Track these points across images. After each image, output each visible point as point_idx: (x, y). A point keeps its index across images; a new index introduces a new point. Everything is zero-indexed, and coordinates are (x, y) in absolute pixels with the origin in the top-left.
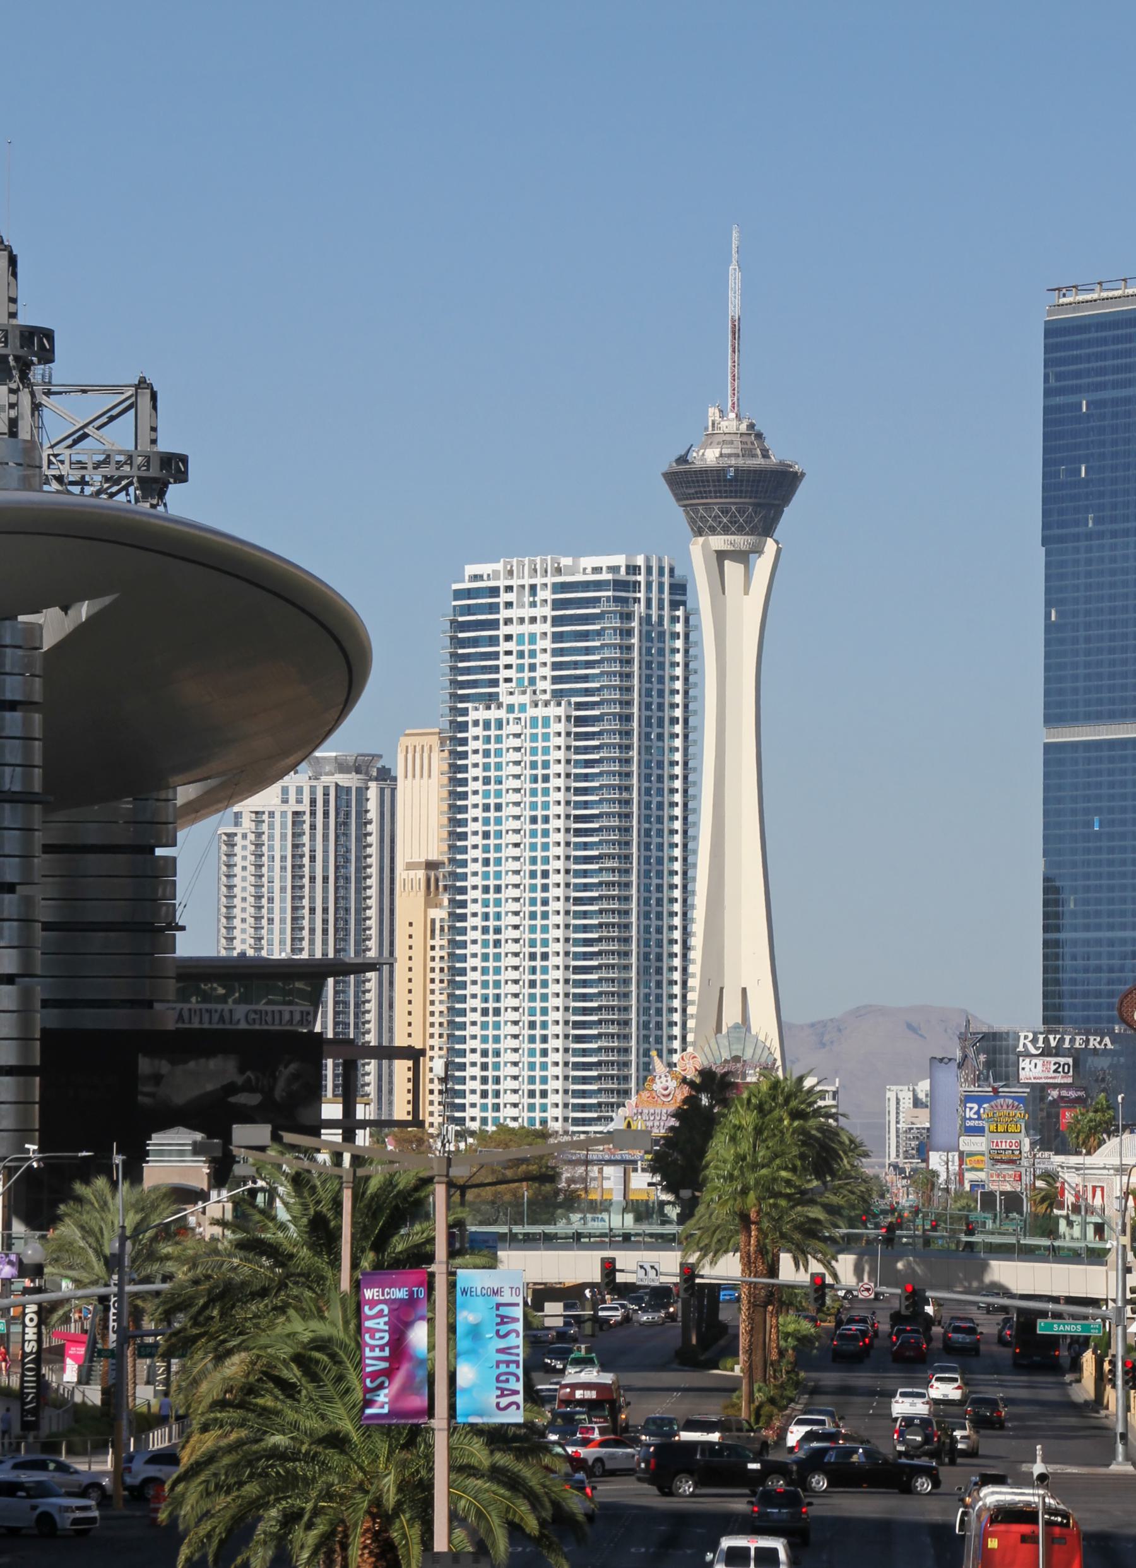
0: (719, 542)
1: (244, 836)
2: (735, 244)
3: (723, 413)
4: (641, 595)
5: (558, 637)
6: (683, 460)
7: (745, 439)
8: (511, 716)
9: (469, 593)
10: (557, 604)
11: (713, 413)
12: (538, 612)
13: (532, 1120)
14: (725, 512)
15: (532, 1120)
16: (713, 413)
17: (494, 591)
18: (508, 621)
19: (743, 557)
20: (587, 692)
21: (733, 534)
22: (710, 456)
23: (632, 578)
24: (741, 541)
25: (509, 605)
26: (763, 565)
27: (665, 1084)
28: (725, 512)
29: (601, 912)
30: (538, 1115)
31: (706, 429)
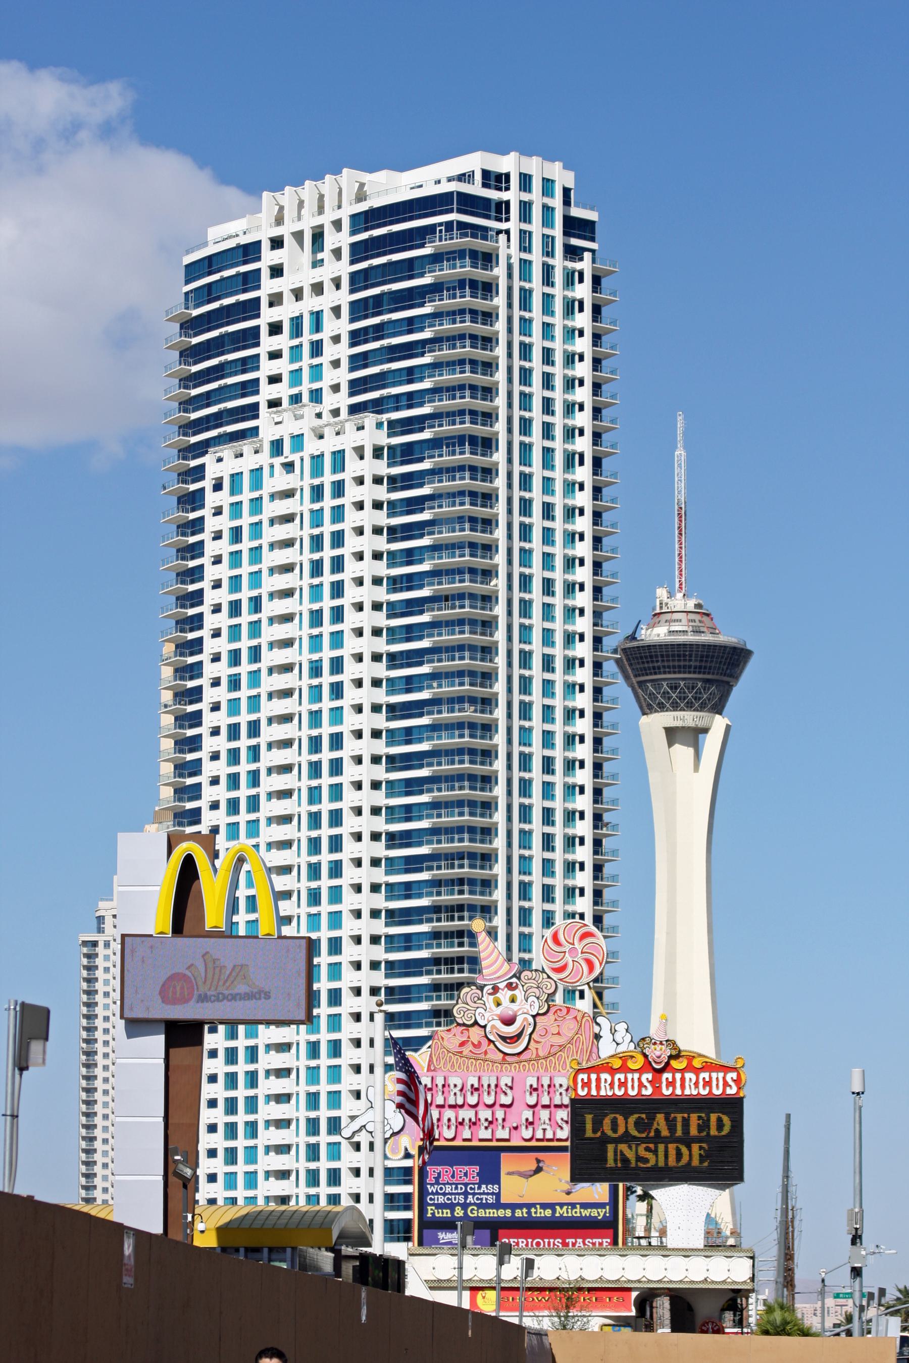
0: (669, 718)
1: (107, 945)
2: (680, 453)
3: (671, 595)
4: (513, 225)
5: (359, 310)
6: (633, 637)
7: (691, 616)
8: (278, 461)
9: (210, 264)
10: (359, 251)
11: (662, 593)
12: (325, 274)
13: (313, 1199)
14: (674, 688)
15: (313, 1199)
16: (662, 593)
17: (250, 251)
18: (275, 300)
19: (693, 736)
20: (411, 399)
21: (682, 710)
22: (658, 634)
23: (493, 195)
24: (688, 718)
25: (277, 271)
26: (712, 743)
27: (507, 1008)
28: (674, 688)
29: (435, 805)
30: (324, 1190)
31: (654, 609)
